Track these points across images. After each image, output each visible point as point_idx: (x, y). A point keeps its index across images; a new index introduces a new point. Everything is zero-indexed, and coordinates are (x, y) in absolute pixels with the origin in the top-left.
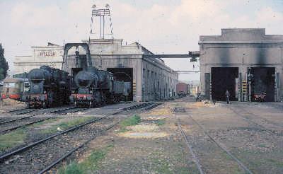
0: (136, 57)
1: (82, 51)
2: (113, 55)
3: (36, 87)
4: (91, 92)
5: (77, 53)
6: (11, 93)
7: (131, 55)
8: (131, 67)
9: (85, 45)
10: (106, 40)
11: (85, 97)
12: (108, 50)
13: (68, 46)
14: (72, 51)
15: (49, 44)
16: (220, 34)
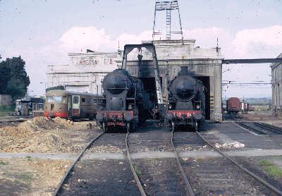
0: (214, 62)
1: (147, 56)
2: (183, 60)
3: (115, 99)
4: (198, 107)
5: (140, 57)
6: (56, 108)
7: (208, 60)
8: (207, 75)
9: (150, 46)
10: (173, 41)
11: (189, 115)
12: (177, 53)
13: (129, 48)
14: (133, 55)
15: (88, 51)
16: (100, 92)
